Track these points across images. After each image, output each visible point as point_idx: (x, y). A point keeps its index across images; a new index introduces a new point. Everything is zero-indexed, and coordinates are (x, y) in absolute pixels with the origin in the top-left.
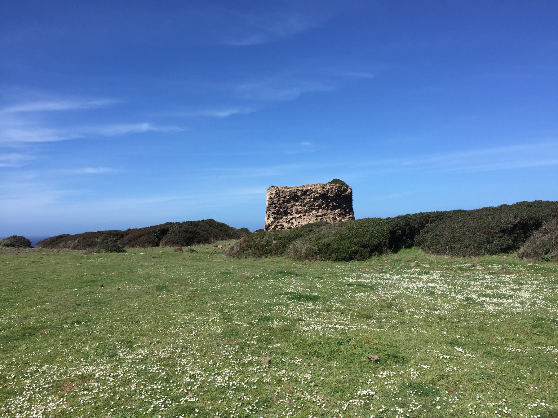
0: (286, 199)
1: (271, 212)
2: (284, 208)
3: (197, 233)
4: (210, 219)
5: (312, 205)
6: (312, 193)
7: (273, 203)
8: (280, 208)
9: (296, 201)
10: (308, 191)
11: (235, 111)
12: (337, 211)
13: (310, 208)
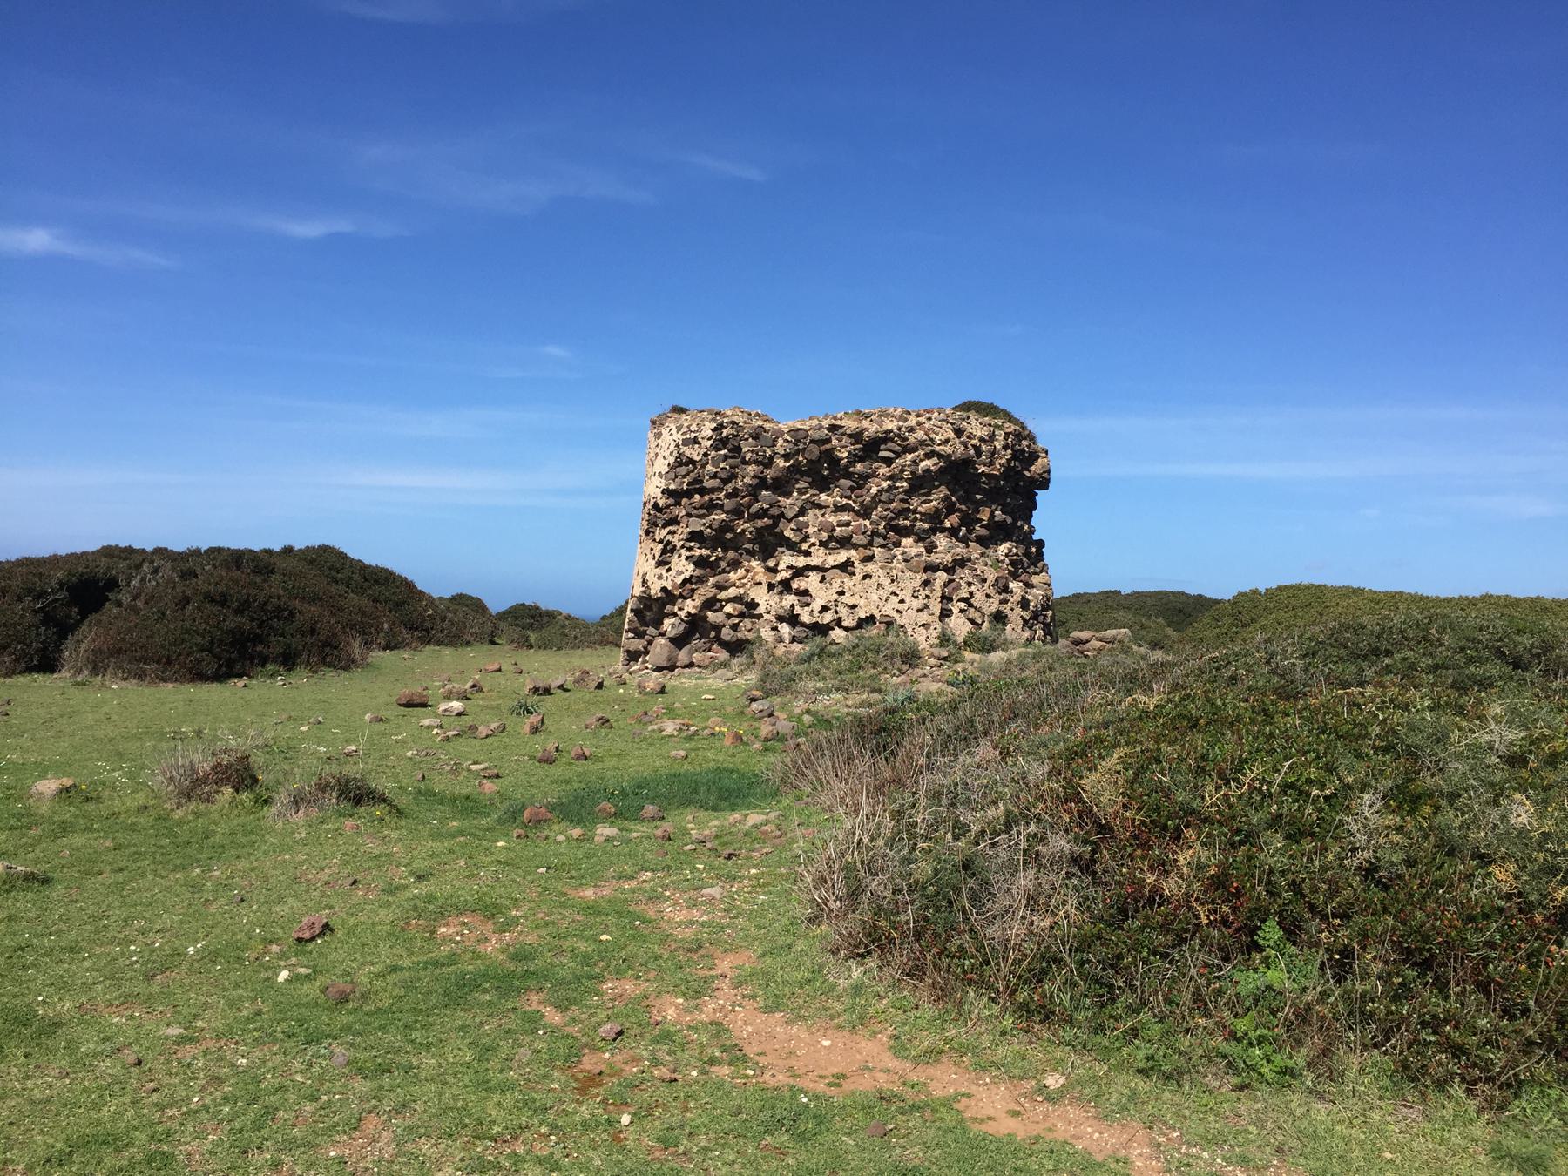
0: (770, 473)
1: (682, 531)
2: (763, 513)
3: (279, 609)
4: (324, 549)
5: (903, 512)
7: (697, 487)
8: (737, 512)
9: (823, 485)
10: (885, 438)
11: (343, 225)
12: (1004, 548)
13: (892, 527)
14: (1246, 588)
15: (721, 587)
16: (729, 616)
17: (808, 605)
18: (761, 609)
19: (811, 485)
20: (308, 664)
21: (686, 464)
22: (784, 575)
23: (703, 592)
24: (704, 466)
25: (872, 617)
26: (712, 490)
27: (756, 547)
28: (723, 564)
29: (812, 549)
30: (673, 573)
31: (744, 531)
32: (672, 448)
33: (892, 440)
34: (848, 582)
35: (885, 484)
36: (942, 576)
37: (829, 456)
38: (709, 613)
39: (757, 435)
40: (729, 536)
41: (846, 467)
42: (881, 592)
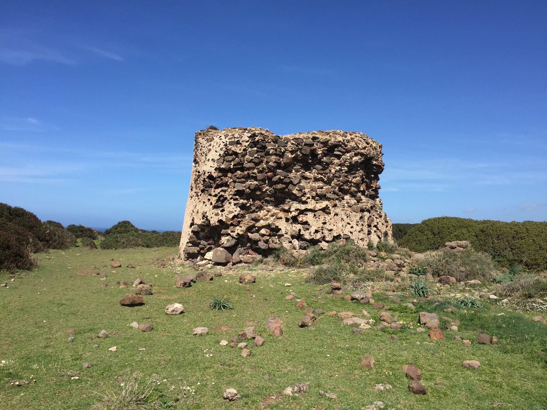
0: (283, 161)
2: (280, 181)
6: (348, 151)
9: (307, 167)
13: (341, 190)
14: (22, 207)
15: (257, 220)
16: (263, 235)
17: (308, 229)
18: (283, 232)
19: (302, 167)
20: (9, 268)
21: (231, 155)
22: (294, 214)
23: (247, 221)
24: (243, 156)
25: (340, 235)
26: (249, 169)
27: (272, 199)
28: (253, 208)
29: (308, 200)
30: (226, 212)
31: (266, 190)
32: (222, 145)
33: (340, 146)
34: (328, 218)
35: (338, 168)
36: (366, 214)
37: (313, 153)
38: (249, 234)
39: (276, 140)
40: (258, 193)
41: (321, 159)
42: (343, 222)
